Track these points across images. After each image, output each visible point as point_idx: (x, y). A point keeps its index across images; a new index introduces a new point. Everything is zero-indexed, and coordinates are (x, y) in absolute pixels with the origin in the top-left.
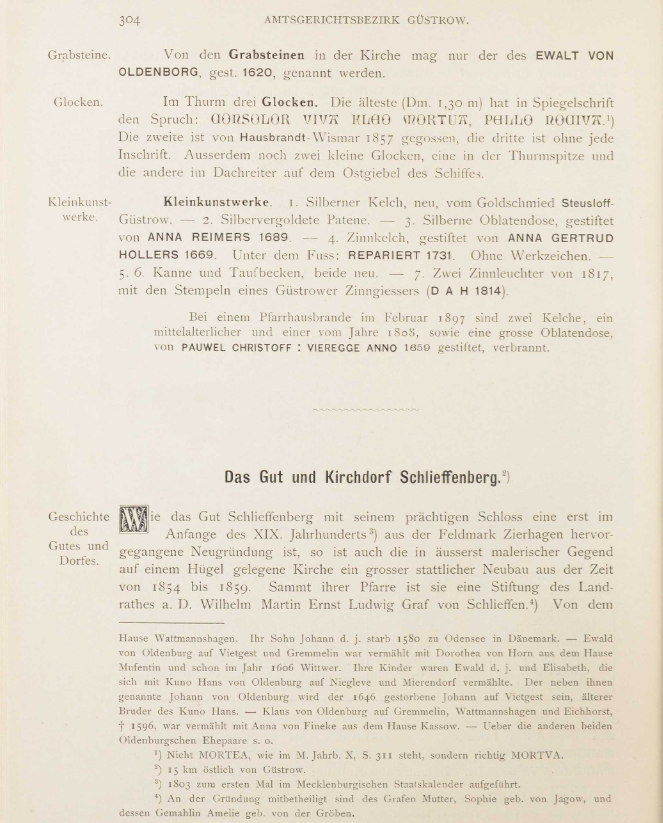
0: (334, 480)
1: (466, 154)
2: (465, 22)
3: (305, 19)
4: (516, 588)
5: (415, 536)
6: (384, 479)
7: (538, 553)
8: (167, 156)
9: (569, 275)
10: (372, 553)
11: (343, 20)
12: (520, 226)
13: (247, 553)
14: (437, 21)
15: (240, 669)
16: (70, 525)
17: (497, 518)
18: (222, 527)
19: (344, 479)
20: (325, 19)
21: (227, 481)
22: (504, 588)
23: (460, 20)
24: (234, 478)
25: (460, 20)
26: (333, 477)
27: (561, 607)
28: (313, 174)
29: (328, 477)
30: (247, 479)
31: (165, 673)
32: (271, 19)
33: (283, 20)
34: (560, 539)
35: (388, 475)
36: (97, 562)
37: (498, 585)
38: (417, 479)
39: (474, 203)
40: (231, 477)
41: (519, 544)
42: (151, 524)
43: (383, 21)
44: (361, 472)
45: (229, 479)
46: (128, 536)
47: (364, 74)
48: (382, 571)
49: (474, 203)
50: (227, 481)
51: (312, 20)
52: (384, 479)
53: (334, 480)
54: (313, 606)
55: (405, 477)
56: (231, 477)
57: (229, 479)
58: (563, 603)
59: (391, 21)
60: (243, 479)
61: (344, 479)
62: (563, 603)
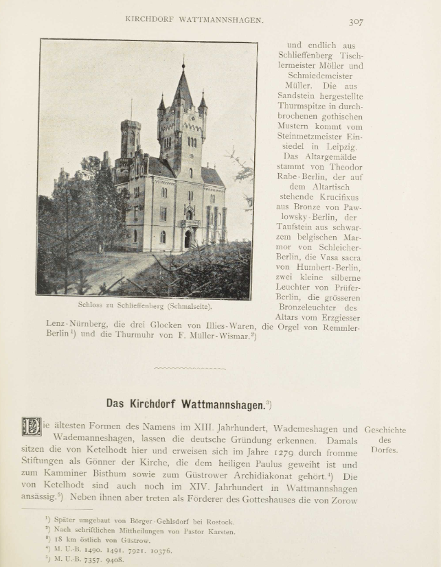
0: (136, 405)
1: (274, 486)
4: (38, 461)
5: (193, 440)
6: (170, 405)
8: (324, 477)
9: (178, 532)
13: (254, 441)
15: (246, 452)
16: (379, 435)
19: (143, 405)
21: (108, 406)
22: (30, 461)
24: (113, 403)
26: (136, 403)
29: (132, 403)
30: (122, 405)
31: (271, 449)
35: (173, 402)
37: (26, 459)
38: (149, 405)
39: (241, 500)
40: (110, 403)
42: (44, 430)
44: (155, 400)
45: (109, 405)
46: (26, 438)
47: (205, 500)
49: (241, 500)
50: (108, 406)
52: (170, 405)
53: (136, 405)
55: (186, 404)
56: (110, 403)
57: (109, 405)
60: (119, 405)
61: (143, 405)
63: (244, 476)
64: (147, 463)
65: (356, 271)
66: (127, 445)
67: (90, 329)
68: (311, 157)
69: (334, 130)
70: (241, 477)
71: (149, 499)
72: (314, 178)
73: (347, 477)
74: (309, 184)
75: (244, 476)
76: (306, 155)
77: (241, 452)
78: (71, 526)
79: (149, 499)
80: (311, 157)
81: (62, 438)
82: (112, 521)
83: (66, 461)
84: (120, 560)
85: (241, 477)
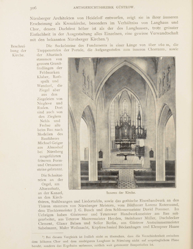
2: (133, 8)
3: (85, 7)
4: (85, 34)
7: (41, 35)
10: (41, 35)
11: (97, 7)
12: (53, 30)
14: (125, 7)
17: (43, 35)
18: (123, 32)
20: (92, 7)
23: (132, 7)
25: (132, 7)
27: (120, 24)
28: (45, 29)
32: (76, 7)
33: (79, 8)
34: (54, 30)
36: (148, 29)
39: (50, 64)
41: (91, 208)
43: (109, 8)
48: (169, 28)
49: (50, 64)
51: (88, 7)
54: (31, 35)
58: (121, 22)
59: (111, 7)
62: (121, 22)
63: (57, 19)
64: (94, 40)
65: (48, 203)
66: (95, 208)
67: (67, 48)
68: (49, 55)
69: (135, 51)
70: (56, 19)
71: (154, 28)
72: (112, 223)
73: (61, 29)
74: (119, 213)
75: (57, 19)
76: (40, 188)
77: (54, 29)
78: (96, 243)
79: (154, 28)
80: (49, 55)
81: (74, 228)
82: (149, 245)
83: (78, 242)
84: (177, 33)
85: (56, 19)
